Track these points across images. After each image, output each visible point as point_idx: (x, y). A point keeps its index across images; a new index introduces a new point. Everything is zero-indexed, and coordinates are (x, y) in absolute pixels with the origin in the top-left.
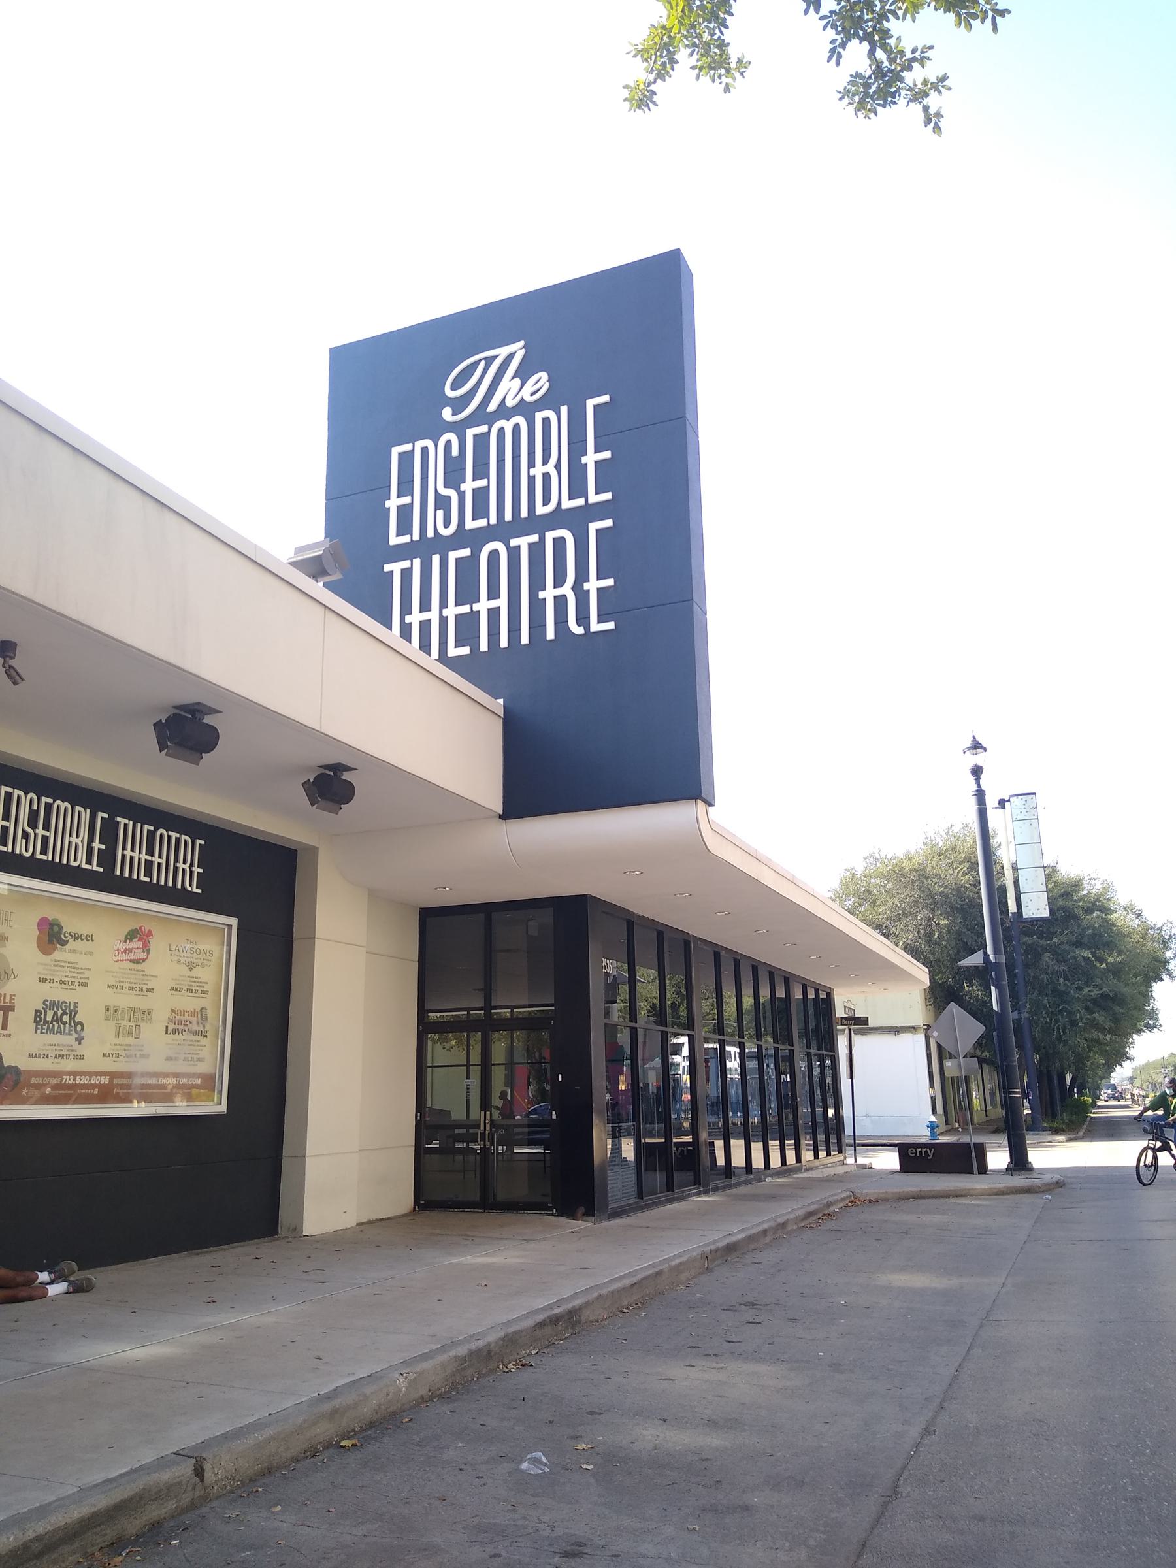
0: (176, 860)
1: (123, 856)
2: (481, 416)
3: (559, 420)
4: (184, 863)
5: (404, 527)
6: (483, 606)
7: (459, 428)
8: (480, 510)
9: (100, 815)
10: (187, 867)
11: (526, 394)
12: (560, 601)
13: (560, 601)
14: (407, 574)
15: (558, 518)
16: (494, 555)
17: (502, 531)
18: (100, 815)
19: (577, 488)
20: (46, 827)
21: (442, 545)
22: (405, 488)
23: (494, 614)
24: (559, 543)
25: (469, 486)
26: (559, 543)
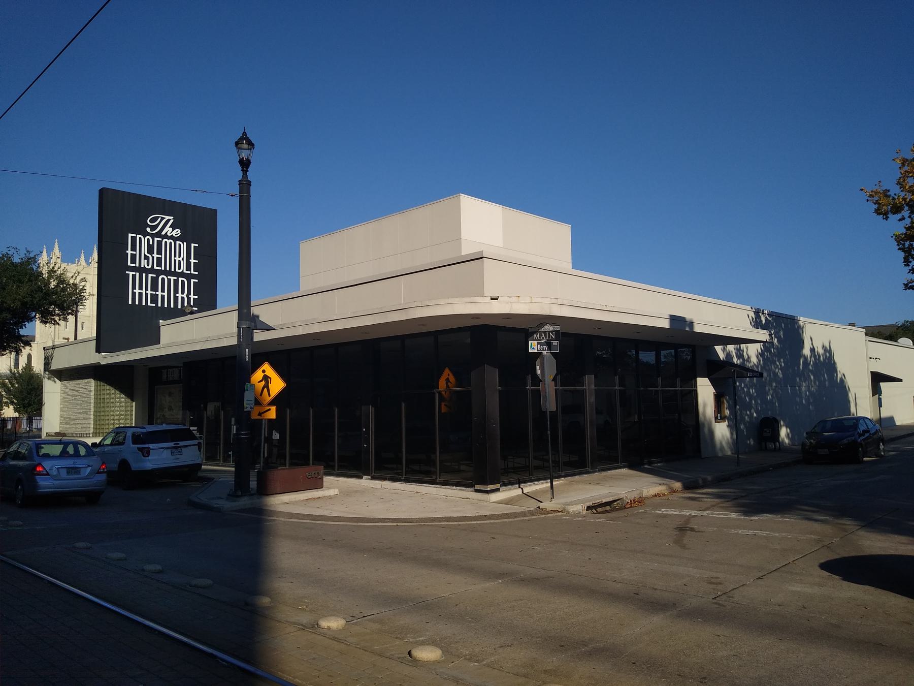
0: (176, 291)
1: (134, 294)
2: (158, 234)
3: (184, 246)
4: (183, 293)
5: (133, 261)
7: (153, 236)
8: (159, 264)
9: (193, 245)
10: (185, 295)
11: (174, 233)
12: (183, 298)
13: (183, 298)
14: (134, 276)
15: (182, 274)
17: (165, 272)
18: (193, 245)
19: (188, 268)
20: (159, 252)
21: (147, 271)
22: (134, 249)
23: (163, 297)
24: (183, 282)
25: (155, 255)
26: (183, 282)
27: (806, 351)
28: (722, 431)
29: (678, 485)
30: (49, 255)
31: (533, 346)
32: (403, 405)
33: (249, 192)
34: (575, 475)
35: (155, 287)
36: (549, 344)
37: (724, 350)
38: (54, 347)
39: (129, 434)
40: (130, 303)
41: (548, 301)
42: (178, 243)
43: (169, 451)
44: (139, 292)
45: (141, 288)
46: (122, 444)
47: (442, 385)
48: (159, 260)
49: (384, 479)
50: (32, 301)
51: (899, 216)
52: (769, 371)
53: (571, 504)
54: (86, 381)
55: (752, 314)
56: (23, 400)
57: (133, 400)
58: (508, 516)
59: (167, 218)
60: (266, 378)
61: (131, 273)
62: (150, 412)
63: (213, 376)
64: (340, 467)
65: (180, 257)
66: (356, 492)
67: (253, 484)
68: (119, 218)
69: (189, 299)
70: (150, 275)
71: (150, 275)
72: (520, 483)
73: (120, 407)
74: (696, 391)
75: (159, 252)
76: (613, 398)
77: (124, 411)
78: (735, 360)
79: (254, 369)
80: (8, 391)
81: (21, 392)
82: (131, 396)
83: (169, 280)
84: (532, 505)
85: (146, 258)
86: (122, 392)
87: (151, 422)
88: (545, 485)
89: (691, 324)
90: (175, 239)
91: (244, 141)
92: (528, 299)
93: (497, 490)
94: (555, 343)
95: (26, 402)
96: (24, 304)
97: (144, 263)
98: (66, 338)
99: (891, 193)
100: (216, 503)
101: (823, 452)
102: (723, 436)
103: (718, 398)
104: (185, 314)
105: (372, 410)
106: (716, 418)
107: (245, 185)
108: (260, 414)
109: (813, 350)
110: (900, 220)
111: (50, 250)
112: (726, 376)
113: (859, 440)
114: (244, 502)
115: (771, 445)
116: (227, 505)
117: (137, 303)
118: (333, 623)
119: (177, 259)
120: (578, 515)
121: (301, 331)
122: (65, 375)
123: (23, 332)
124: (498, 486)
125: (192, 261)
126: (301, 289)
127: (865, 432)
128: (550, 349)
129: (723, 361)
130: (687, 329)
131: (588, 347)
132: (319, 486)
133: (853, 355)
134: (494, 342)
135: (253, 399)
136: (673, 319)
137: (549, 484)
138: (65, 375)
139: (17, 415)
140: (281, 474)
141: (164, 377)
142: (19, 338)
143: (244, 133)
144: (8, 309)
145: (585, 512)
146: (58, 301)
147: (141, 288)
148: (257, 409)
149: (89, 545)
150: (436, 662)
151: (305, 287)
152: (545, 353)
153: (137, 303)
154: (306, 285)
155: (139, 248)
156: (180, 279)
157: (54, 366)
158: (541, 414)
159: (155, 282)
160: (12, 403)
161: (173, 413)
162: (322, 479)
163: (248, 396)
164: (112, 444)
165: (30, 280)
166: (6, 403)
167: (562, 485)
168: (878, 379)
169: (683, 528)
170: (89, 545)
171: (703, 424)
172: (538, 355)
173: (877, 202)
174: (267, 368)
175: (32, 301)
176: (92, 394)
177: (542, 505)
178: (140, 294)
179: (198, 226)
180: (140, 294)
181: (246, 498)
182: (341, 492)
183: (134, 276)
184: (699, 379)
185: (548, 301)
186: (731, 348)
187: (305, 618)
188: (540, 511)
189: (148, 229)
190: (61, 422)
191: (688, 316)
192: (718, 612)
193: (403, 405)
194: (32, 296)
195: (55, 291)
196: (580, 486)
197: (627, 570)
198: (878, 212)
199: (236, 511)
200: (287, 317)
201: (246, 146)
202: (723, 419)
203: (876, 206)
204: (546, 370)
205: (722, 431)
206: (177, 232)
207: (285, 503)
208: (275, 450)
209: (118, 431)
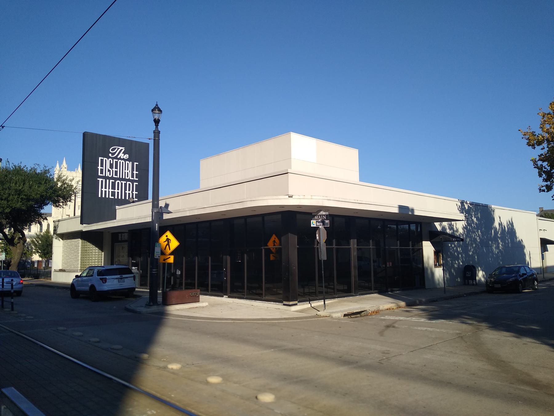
0: (125, 190)
1: (102, 191)
2: (116, 158)
3: (130, 164)
4: (129, 190)
5: (102, 173)
6: (116, 191)
8: (116, 174)
9: (135, 163)
10: (130, 192)
11: (125, 157)
12: (129, 194)
13: (129, 194)
14: (102, 181)
15: (129, 180)
16: (118, 183)
17: (119, 179)
18: (135, 163)
19: (133, 176)
20: (116, 168)
22: (102, 166)
23: (118, 193)
24: (129, 184)
25: (114, 169)
26: (129, 184)
27: (496, 224)
28: (439, 273)
29: (403, 304)
30: (60, 166)
31: (314, 223)
32: (210, 258)
33: (159, 137)
34: (344, 297)
35: (113, 188)
36: (323, 222)
37: (440, 225)
38: (59, 221)
39: (96, 271)
40: (100, 196)
41: (322, 198)
42: (127, 162)
43: (117, 280)
44: (105, 190)
45: (106, 188)
46: (92, 276)
47: (270, 245)
48: (116, 172)
49: (235, 297)
50: (46, 195)
51: (541, 147)
52: (471, 237)
53: (333, 313)
54: (76, 240)
55: (459, 204)
56: (44, 250)
57: (102, 251)
58: (297, 318)
59: (121, 148)
60: (168, 240)
61: (100, 180)
62: (111, 258)
63: (140, 238)
64: (212, 290)
65: (128, 170)
66: (218, 304)
67: (160, 299)
68: (94, 148)
69: (133, 194)
70: (111, 181)
71: (111, 181)
72: (310, 300)
73: (95, 255)
74: (422, 249)
75: (116, 168)
76: (369, 253)
77: (97, 257)
78: (448, 231)
79: (161, 235)
80: (35, 245)
81: (43, 246)
82: (101, 248)
83: (122, 183)
84: (314, 312)
85: (109, 171)
86: (96, 246)
87: (112, 264)
88: (321, 303)
89: (413, 210)
90: (125, 160)
91: (157, 109)
92: (310, 197)
93: (296, 304)
94: (327, 221)
95: (46, 251)
96: (42, 196)
97: (108, 174)
98: (63, 216)
99: (537, 133)
100: (138, 309)
101: (497, 286)
102: (440, 276)
103: (436, 253)
104: (130, 203)
105: (228, 258)
106: (435, 266)
107: (157, 133)
108: (164, 260)
109: (500, 224)
110: (542, 149)
111: (61, 164)
112: (441, 240)
113: (520, 279)
114: (154, 308)
115: (471, 282)
116: (144, 310)
117: (103, 196)
118: (175, 366)
119: (126, 171)
120: (339, 319)
121: (188, 214)
122: (66, 236)
123: (42, 211)
124: (296, 302)
125: (135, 172)
126: (201, 187)
127: (524, 274)
128: (324, 224)
129: (440, 232)
130: (410, 213)
131: (347, 224)
132: (198, 301)
133: (529, 229)
134: (293, 221)
135: (160, 251)
136: (401, 207)
137: (323, 303)
138: (66, 236)
139: (40, 259)
140: (175, 294)
141: (120, 238)
142: (41, 215)
143: (157, 105)
144: (33, 200)
145: (342, 317)
146: (60, 195)
147: (106, 188)
148: (163, 257)
149: (65, 329)
150: (218, 384)
151: (203, 186)
152: (320, 227)
153: (103, 196)
154: (204, 185)
155: (105, 166)
156: (128, 183)
157: (59, 231)
158: (319, 261)
159: (114, 184)
160: (38, 252)
161: (123, 258)
162: (199, 297)
163: (157, 250)
164: (86, 276)
165: (45, 183)
166: (34, 252)
167: (329, 303)
168: (545, 243)
169: (390, 326)
170: (65, 329)
171: (427, 269)
172: (317, 228)
173: (528, 139)
174: (169, 234)
175: (46, 195)
176: (80, 248)
177: (319, 313)
178: (105, 191)
179: (137, 152)
180: (105, 191)
181: (155, 307)
182: (209, 304)
183: (102, 181)
184: (424, 242)
185: (322, 198)
186: (445, 224)
187: (162, 365)
188: (318, 316)
189: (110, 155)
190: (63, 263)
191: (410, 206)
192: (381, 367)
193: (210, 258)
194: (47, 192)
195: (60, 189)
196: (345, 303)
197: (344, 346)
198: (529, 144)
199: (150, 313)
200: (183, 205)
201: (157, 112)
202: (440, 266)
203: (527, 141)
204: (321, 237)
205: (439, 273)
206: (126, 156)
207: (177, 309)
208: (178, 281)
209: (91, 269)
